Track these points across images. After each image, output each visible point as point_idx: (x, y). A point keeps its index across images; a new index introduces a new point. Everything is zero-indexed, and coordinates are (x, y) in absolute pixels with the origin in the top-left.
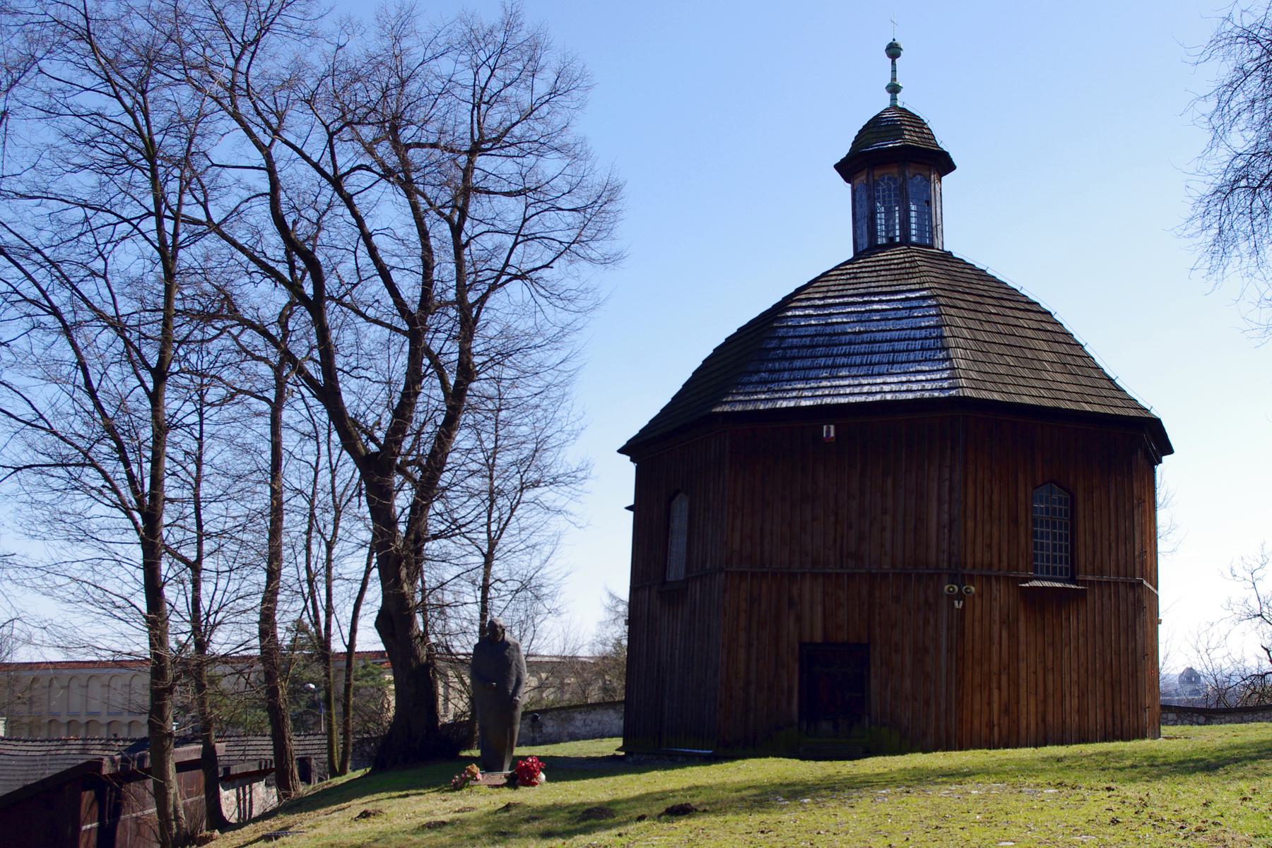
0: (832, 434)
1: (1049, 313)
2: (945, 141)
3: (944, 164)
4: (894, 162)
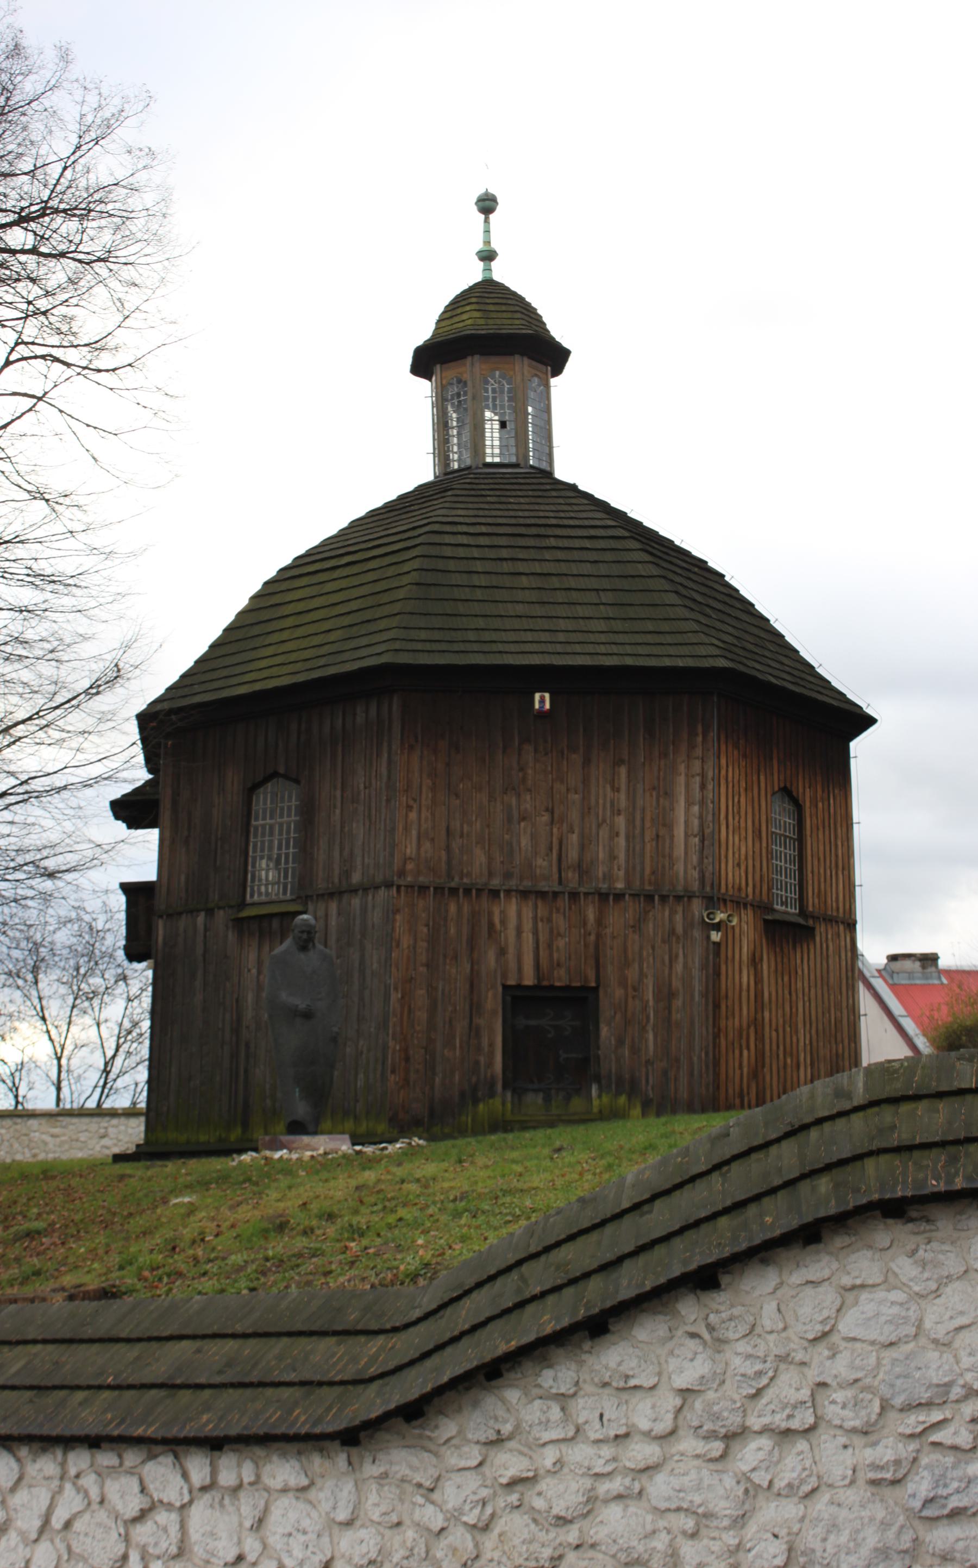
0: (547, 706)
2: (559, 330)
3: (553, 357)
4: (490, 345)
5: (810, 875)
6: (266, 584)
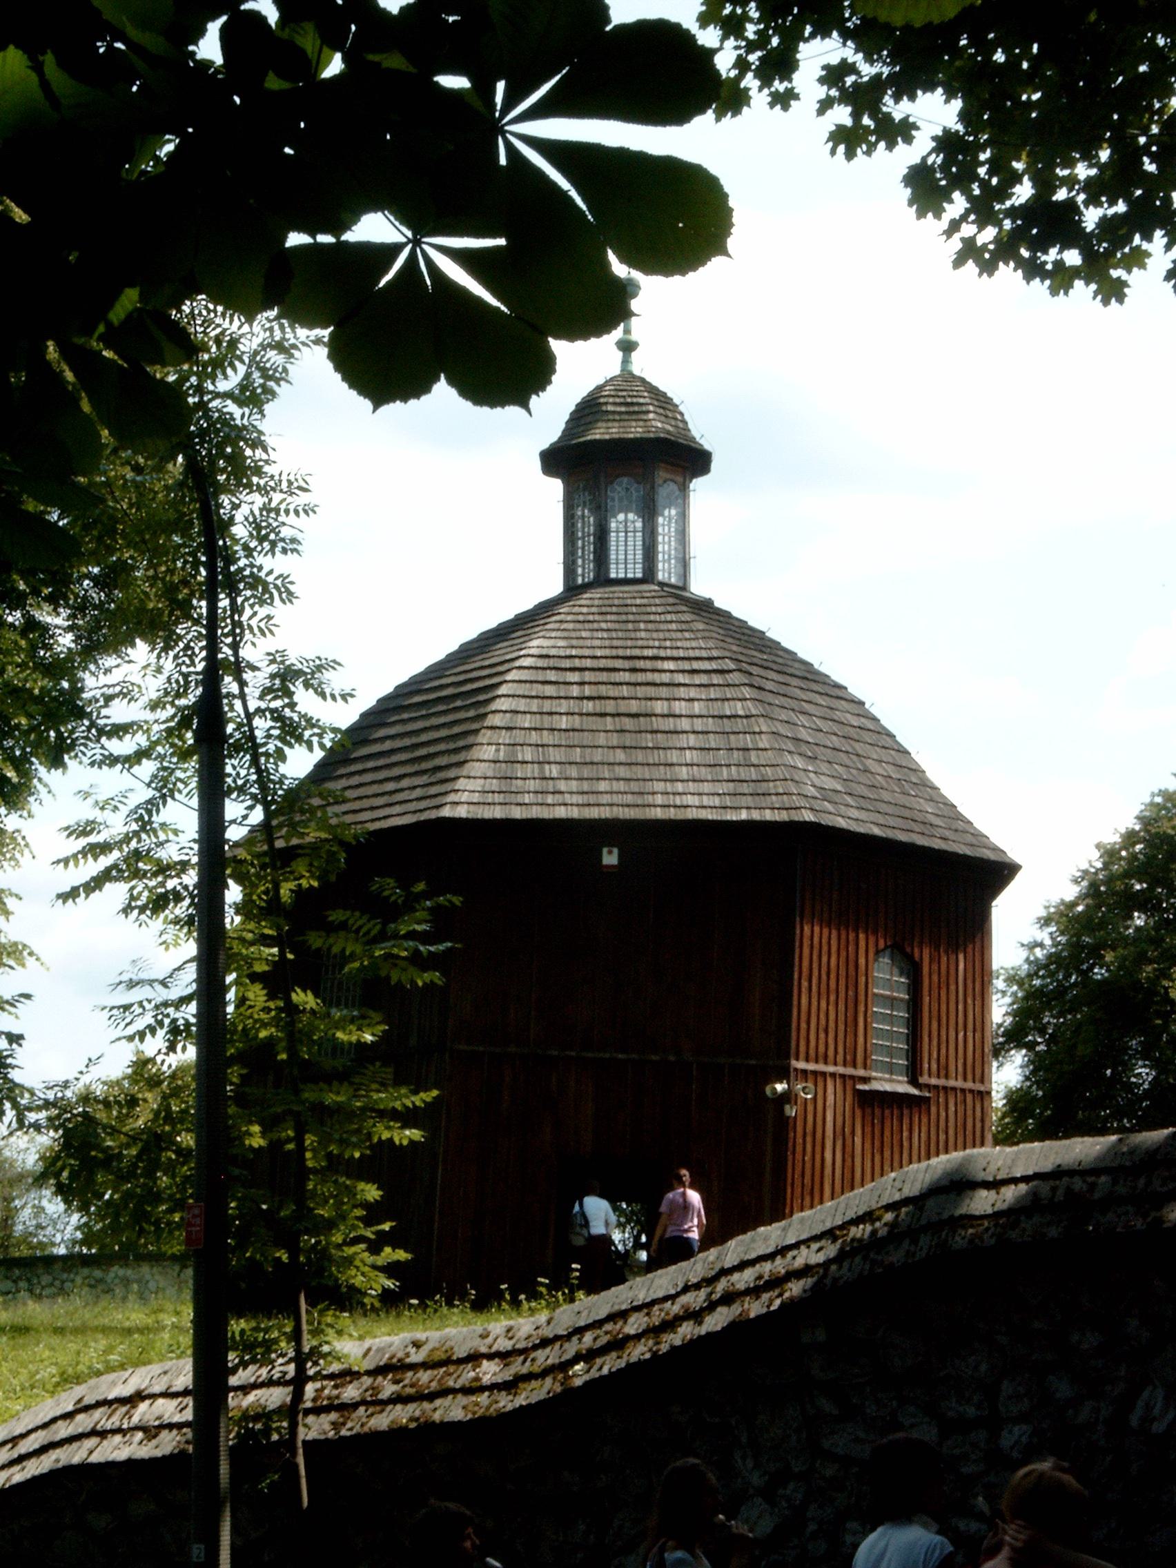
1: (862, 703)
2: (703, 431)
3: (690, 460)
5: (926, 1039)
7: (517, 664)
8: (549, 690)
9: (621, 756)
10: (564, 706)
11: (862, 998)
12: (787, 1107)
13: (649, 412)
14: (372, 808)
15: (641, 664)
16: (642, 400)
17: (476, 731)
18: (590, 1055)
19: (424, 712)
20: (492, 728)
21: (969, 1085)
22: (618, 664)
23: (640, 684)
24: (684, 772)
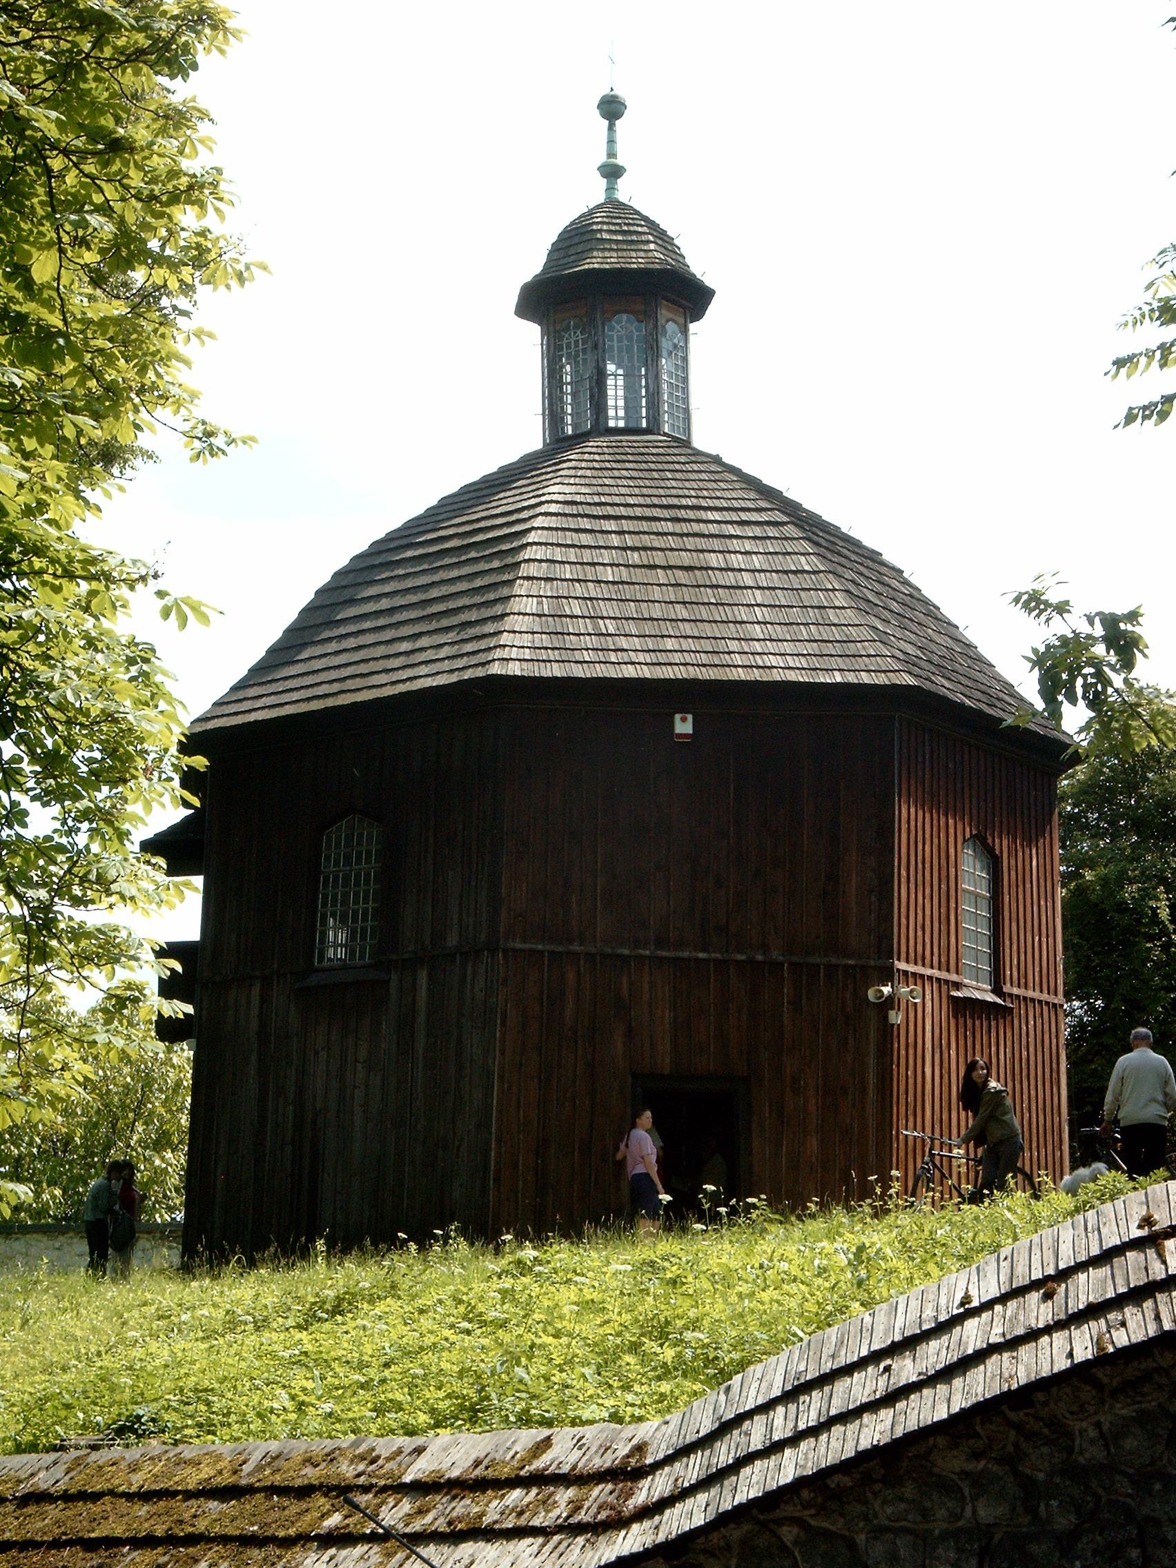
2: (700, 265)
3: (690, 297)
4: (611, 297)
5: (1007, 942)
6: (338, 575)
7: (543, 509)
8: (586, 539)
9: (682, 612)
10: (606, 557)
11: (952, 892)
12: (892, 1014)
13: (648, 242)
14: (387, 671)
15: (682, 514)
16: (640, 229)
17: (510, 583)
18: (664, 954)
19: (426, 566)
20: (528, 578)
21: (1044, 997)
22: (657, 513)
23: (688, 535)
24: (758, 631)
